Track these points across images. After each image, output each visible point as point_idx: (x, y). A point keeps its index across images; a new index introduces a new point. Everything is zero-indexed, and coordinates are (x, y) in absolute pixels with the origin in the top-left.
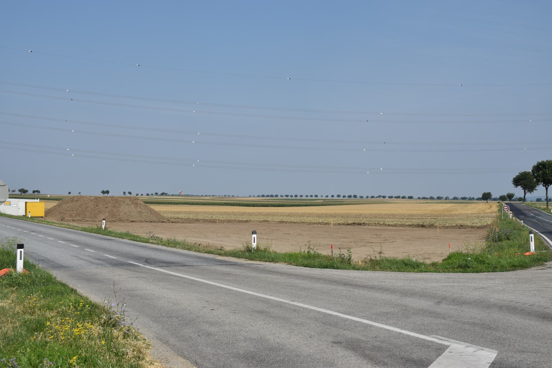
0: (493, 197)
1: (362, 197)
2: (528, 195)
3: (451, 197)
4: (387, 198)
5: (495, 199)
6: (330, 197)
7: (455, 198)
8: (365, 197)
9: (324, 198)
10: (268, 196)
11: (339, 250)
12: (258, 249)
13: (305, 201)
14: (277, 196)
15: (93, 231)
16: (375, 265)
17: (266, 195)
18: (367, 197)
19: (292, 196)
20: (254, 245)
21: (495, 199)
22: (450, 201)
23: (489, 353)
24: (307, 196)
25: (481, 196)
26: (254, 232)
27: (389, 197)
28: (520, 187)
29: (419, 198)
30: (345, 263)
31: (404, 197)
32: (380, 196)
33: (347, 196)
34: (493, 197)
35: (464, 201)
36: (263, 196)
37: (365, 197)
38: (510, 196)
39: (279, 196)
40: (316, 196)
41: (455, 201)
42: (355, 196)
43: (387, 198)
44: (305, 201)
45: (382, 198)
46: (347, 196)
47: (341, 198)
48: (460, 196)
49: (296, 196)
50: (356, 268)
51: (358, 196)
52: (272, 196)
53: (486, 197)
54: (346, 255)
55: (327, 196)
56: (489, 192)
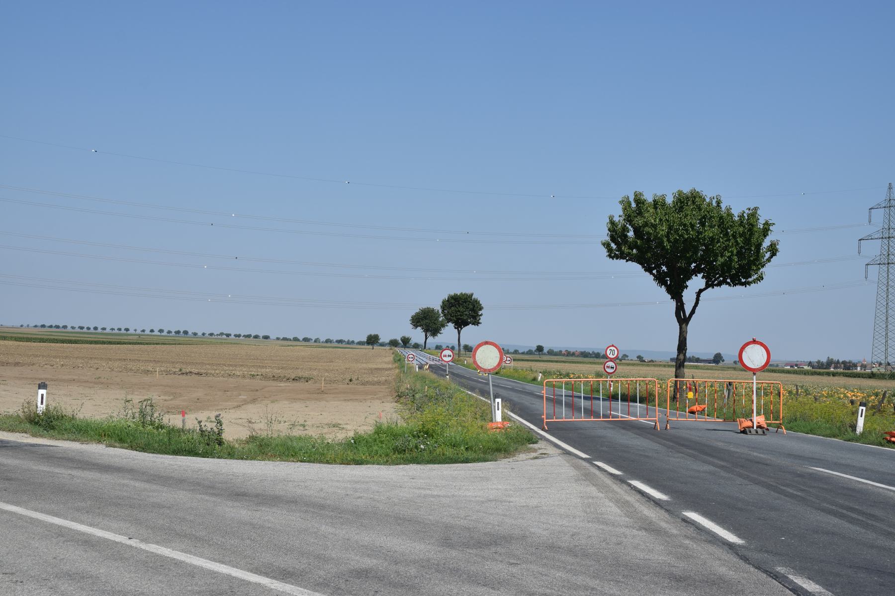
0: (380, 341)
1: (195, 334)
2: (431, 339)
3: (323, 339)
4: (232, 336)
5: (382, 345)
6: (156, 333)
7: (328, 341)
8: (200, 334)
9: (139, 332)
10: (51, 327)
11: (180, 417)
12: (47, 413)
13: (126, 337)
14: (65, 327)
15: (330, 455)
16: (261, 448)
17: (47, 324)
18: (204, 334)
19: (88, 328)
20: (41, 408)
21: (382, 345)
22: (333, 345)
23: (20, 441)
24: (112, 329)
25: (365, 340)
26: (42, 386)
27: (236, 336)
28: (419, 328)
29: (278, 339)
30: (211, 444)
31: (256, 337)
32: (222, 334)
33: (173, 331)
34: (380, 341)
35: (340, 345)
36: (43, 326)
37: (200, 334)
38: (406, 342)
39: (69, 327)
40: (127, 330)
41: (329, 344)
42: (186, 332)
43: (232, 336)
44: (126, 337)
45: (224, 337)
46: (173, 331)
47: (165, 333)
48: (335, 338)
49: (96, 328)
50: (231, 454)
51: (190, 333)
52: (57, 327)
53: (373, 340)
54: (216, 430)
55: (143, 331)
56: (482, 319)
